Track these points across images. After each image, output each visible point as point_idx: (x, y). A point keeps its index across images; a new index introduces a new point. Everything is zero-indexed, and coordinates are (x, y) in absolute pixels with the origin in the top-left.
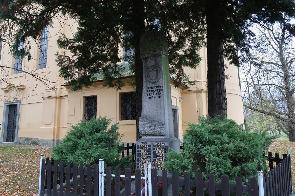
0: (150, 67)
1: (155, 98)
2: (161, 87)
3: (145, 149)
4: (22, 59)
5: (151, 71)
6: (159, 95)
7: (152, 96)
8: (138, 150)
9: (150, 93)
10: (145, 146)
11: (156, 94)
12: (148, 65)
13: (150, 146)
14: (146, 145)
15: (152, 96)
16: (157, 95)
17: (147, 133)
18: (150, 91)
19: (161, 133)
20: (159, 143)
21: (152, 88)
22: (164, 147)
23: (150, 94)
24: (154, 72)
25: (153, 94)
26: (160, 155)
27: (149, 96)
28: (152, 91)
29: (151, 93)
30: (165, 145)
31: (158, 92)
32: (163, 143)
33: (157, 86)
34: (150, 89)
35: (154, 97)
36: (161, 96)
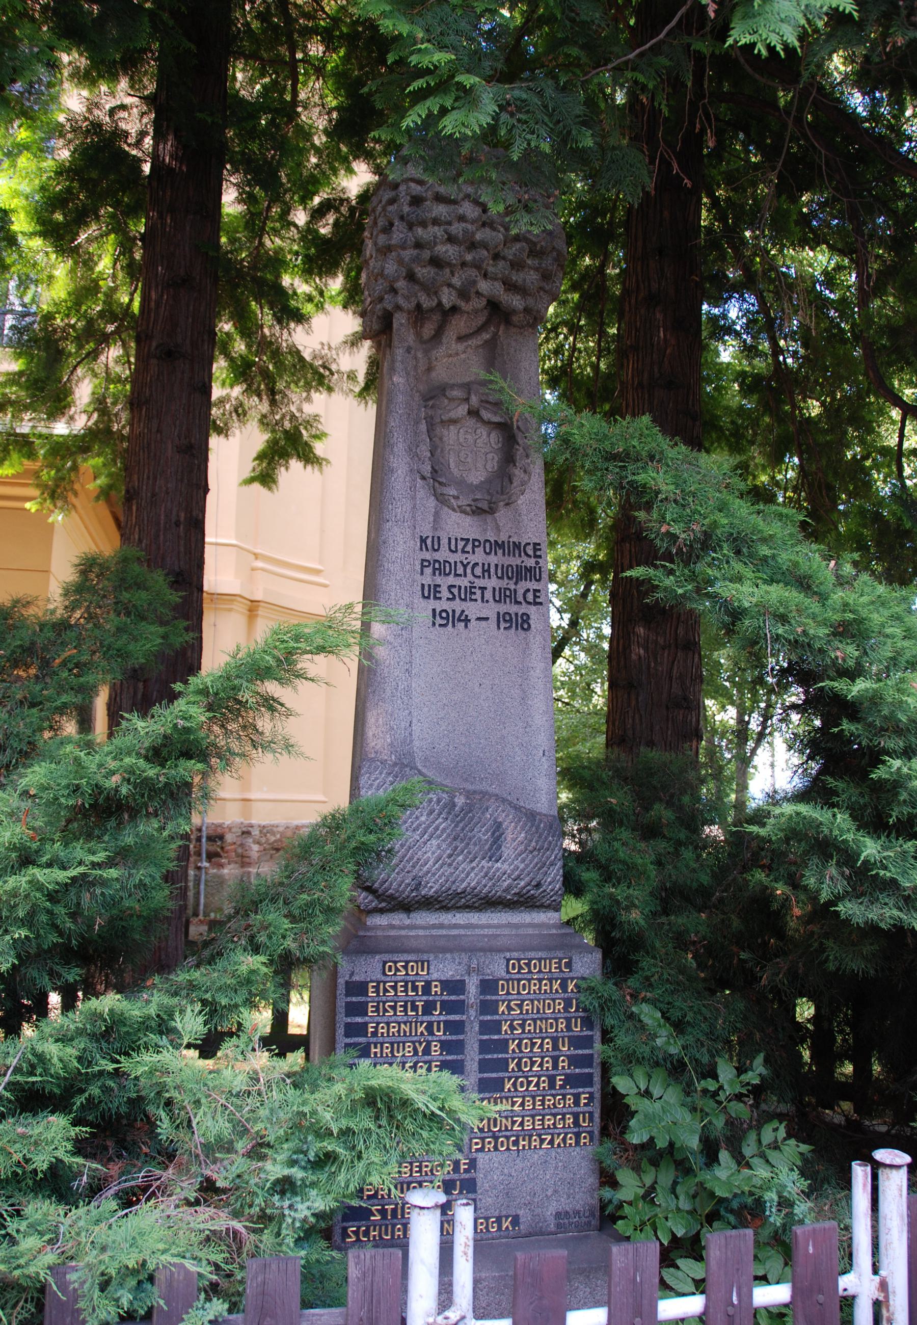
0: (456, 393)
1: (484, 623)
2: (531, 552)
3: (415, 1008)
4: (421, 327)
5: (454, 421)
6: (513, 609)
7: (458, 605)
8: (359, 1020)
9: (444, 582)
10: (415, 988)
11: (488, 595)
12: (434, 374)
13: (454, 986)
14: (428, 985)
15: (458, 605)
16: (503, 608)
17: (431, 888)
18: (440, 568)
19: (538, 885)
20: (528, 965)
21: (461, 544)
22: (564, 986)
23: (445, 594)
24: (483, 431)
25: (468, 594)
26: (533, 1044)
27: (439, 606)
28: (460, 571)
29: (451, 580)
30: (571, 975)
31: (504, 583)
32: (561, 960)
33: (503, 537)
34: (443, 554)
35: (472, 617)
36: (526, 618)
